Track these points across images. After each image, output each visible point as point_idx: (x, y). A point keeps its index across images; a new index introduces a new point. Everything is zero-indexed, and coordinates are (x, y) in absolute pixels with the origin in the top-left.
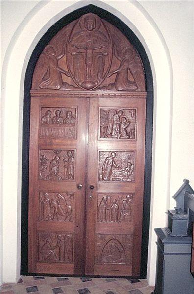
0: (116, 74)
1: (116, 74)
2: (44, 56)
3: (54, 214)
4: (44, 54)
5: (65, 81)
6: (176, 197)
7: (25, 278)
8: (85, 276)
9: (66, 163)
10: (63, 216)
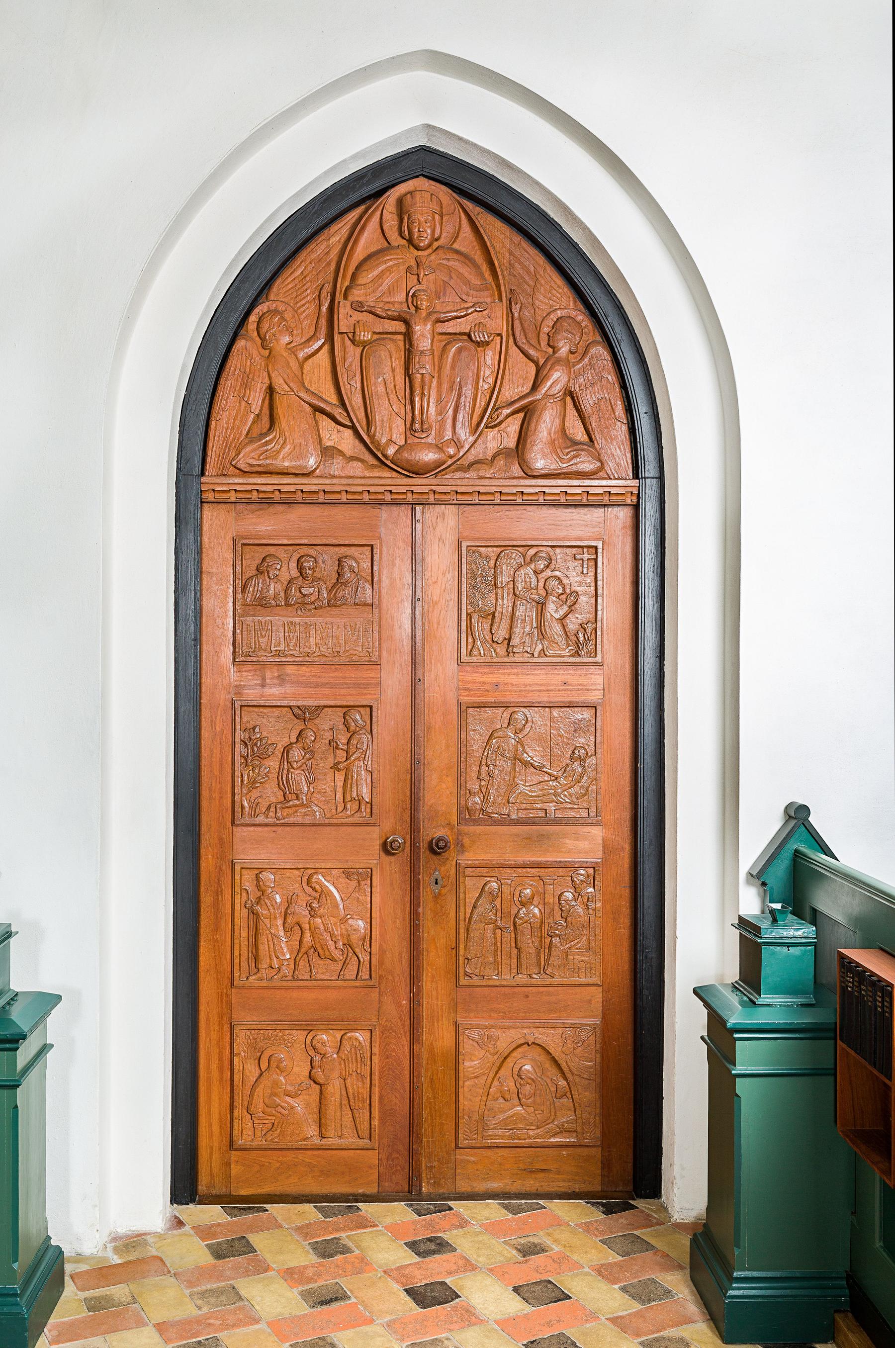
0: (522, 415)
1: (522, 415)
2: (249, 344)
3: (299, 953)
4: (252, 340)
5: (328, 444)
6: (759, 877)
7: (193, 1212)
8: (420, 1197)
9: (341, 756)
10: (333, 959)
